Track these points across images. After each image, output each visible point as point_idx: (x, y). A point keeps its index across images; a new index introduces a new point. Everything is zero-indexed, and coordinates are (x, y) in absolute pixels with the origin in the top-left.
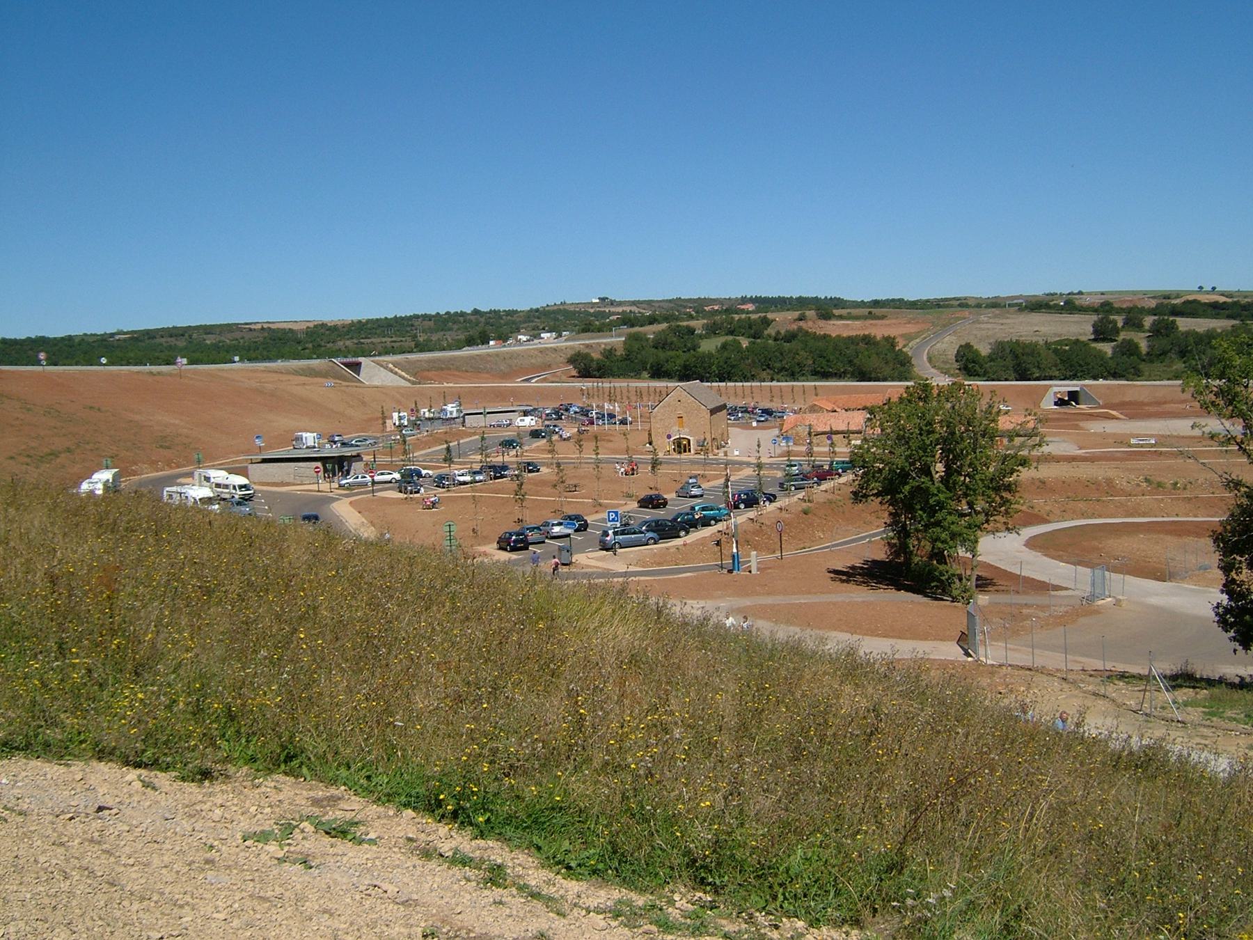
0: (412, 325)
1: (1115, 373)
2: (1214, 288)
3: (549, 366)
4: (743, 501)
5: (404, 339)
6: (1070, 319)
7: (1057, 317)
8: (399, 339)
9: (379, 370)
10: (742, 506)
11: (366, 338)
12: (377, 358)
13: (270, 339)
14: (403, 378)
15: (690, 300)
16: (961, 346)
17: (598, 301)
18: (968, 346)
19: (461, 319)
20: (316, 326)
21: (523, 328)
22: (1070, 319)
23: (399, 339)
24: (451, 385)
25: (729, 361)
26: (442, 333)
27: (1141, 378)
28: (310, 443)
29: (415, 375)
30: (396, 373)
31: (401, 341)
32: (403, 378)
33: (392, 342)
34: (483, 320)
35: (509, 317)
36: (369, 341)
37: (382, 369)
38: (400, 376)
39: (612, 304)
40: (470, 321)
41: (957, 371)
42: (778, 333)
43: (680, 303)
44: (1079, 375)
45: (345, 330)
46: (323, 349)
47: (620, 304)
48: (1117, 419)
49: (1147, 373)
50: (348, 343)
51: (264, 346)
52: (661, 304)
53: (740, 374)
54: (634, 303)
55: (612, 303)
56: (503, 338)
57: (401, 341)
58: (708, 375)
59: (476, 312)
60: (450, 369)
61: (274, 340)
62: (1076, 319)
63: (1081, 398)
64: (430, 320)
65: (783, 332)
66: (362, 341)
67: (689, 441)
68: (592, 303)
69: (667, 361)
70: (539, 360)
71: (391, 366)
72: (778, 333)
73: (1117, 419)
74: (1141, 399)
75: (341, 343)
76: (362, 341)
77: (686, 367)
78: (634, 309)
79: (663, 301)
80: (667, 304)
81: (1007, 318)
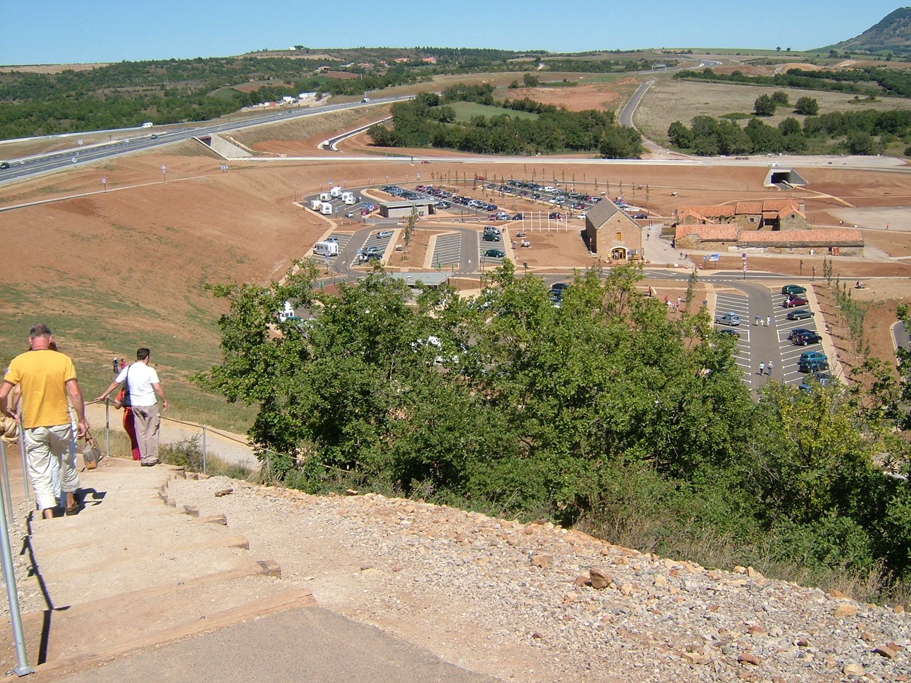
0: (148, 72)
1: (788, 148)
2: (789, 49)
3: (335, 131)
4: (807, 340)
5: (153, 88)
6: (716, 88)
7: (720, 87)
8: (150, 88)
9: (226, 144)
10: (806, 344)
11: (121, 87)
12: (222, 132)
13: (26, 84)
14: (245, 149)
15: (372, 50)
16: (673, 124)
17: (294, 49)
18: (678, 123)
19: (189, 67)
20: (64, 73)
21: (251, 78)
22: (716, 88)
23: (150, 88)
24: (283, 158)
25: (502, 136)
26: (185, 82)
27: (806, 152)
28: (333, 252)
29: (250, 146)
30: (238, 146)
31: (152, 90)
32: (245, 149)
33: (143, 90)
34: (207, 67)
35: (229, 65)
36: (124, 89)
37: (228, 143)
38: (242, 148)
39: (307, 52)
40: (197, 69)
41: (670, 144)
42: (507, 101)
43: (365, 52)
44: (763, 149)
45: (91, 76)
46: (85, 97)
47: (314, 52)
48: (848, 207)
49: (811, 149)
50: (106, 91)
51: (22, 90)
52: (350, 53)
53: (511, 146)
54: (326, 52)
55: (308, 51)
56: (273, 100)
57: (152, 90)
58: (486, 147)
59: (200, 60)
60: (271, 139)
61: (30, 85)
62: (723, 89)
63: (791, 178)
64: (162, 67)
65: (511, 101)
66: (118, 89)
67: (624, 250)
68: (289, 51)
69: (449, 134)
70: (326, 126)
71: (232, 139)
72: (507, 101)
73: (848, 207)
74: (838, 181)
75: (100, 91)
76: (118, 89)
77: (467, 140)
78: (327, 56)
79: (350, 50)
80: (354, 53)
81: (669, 86)
